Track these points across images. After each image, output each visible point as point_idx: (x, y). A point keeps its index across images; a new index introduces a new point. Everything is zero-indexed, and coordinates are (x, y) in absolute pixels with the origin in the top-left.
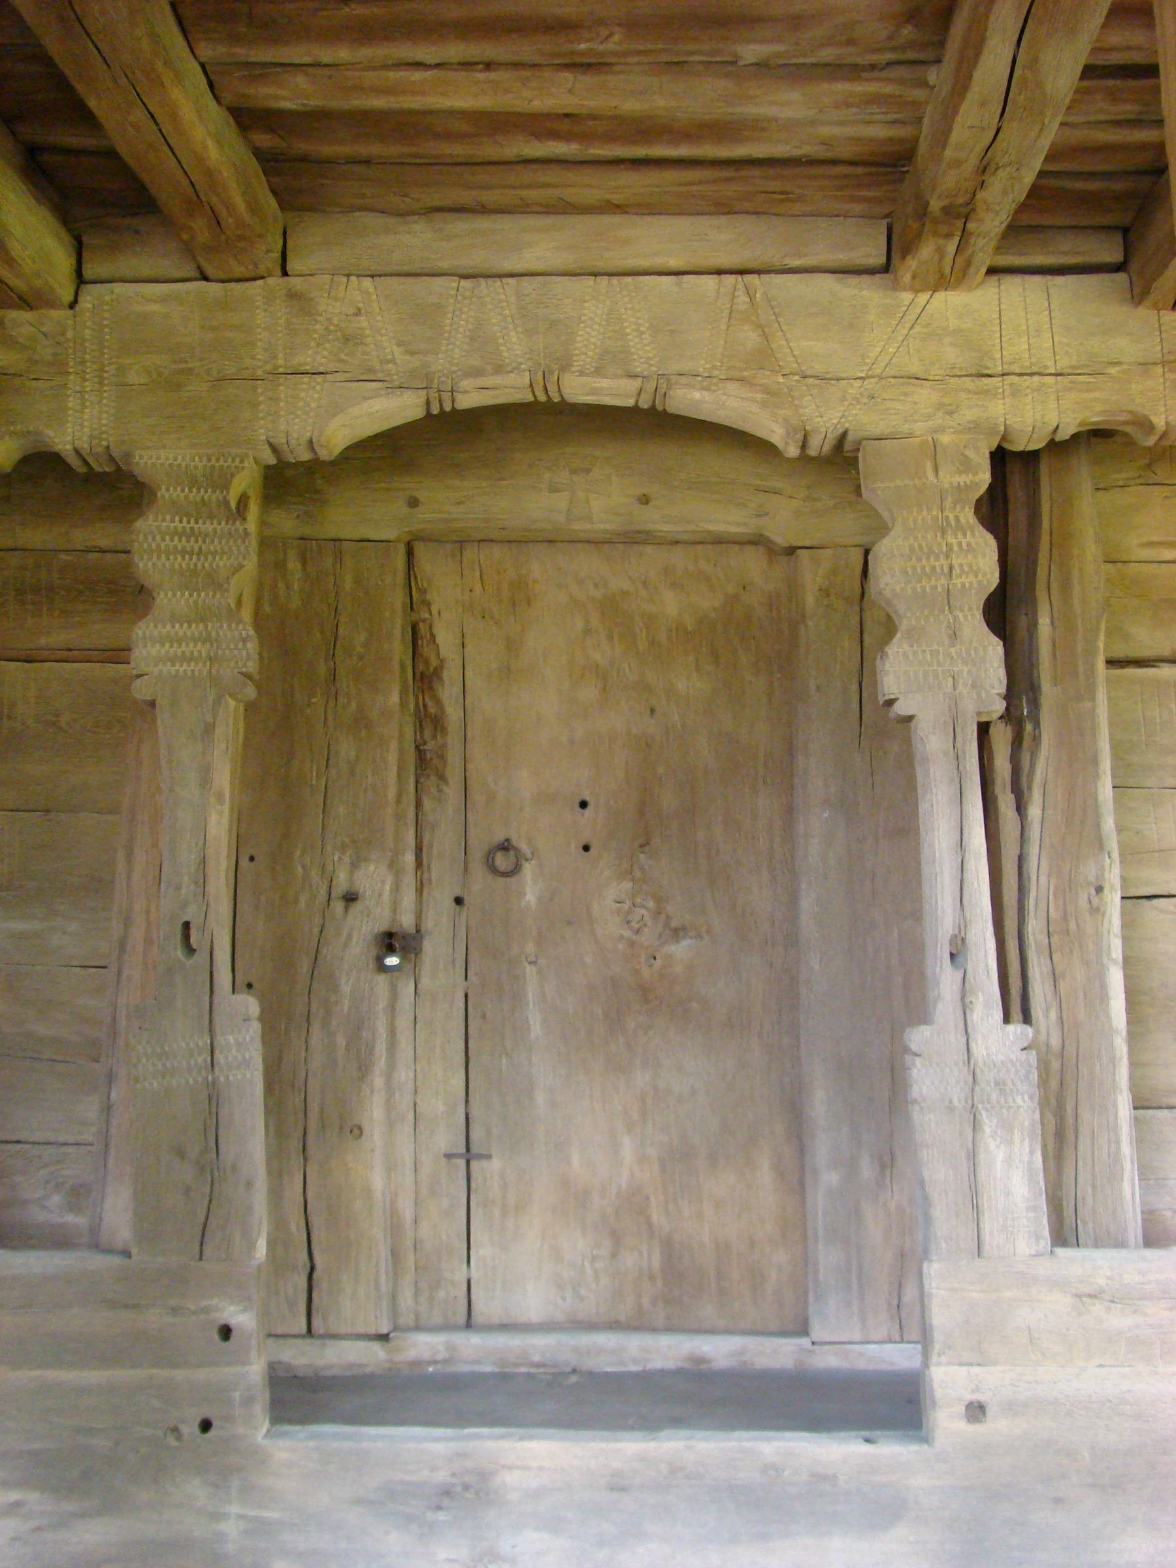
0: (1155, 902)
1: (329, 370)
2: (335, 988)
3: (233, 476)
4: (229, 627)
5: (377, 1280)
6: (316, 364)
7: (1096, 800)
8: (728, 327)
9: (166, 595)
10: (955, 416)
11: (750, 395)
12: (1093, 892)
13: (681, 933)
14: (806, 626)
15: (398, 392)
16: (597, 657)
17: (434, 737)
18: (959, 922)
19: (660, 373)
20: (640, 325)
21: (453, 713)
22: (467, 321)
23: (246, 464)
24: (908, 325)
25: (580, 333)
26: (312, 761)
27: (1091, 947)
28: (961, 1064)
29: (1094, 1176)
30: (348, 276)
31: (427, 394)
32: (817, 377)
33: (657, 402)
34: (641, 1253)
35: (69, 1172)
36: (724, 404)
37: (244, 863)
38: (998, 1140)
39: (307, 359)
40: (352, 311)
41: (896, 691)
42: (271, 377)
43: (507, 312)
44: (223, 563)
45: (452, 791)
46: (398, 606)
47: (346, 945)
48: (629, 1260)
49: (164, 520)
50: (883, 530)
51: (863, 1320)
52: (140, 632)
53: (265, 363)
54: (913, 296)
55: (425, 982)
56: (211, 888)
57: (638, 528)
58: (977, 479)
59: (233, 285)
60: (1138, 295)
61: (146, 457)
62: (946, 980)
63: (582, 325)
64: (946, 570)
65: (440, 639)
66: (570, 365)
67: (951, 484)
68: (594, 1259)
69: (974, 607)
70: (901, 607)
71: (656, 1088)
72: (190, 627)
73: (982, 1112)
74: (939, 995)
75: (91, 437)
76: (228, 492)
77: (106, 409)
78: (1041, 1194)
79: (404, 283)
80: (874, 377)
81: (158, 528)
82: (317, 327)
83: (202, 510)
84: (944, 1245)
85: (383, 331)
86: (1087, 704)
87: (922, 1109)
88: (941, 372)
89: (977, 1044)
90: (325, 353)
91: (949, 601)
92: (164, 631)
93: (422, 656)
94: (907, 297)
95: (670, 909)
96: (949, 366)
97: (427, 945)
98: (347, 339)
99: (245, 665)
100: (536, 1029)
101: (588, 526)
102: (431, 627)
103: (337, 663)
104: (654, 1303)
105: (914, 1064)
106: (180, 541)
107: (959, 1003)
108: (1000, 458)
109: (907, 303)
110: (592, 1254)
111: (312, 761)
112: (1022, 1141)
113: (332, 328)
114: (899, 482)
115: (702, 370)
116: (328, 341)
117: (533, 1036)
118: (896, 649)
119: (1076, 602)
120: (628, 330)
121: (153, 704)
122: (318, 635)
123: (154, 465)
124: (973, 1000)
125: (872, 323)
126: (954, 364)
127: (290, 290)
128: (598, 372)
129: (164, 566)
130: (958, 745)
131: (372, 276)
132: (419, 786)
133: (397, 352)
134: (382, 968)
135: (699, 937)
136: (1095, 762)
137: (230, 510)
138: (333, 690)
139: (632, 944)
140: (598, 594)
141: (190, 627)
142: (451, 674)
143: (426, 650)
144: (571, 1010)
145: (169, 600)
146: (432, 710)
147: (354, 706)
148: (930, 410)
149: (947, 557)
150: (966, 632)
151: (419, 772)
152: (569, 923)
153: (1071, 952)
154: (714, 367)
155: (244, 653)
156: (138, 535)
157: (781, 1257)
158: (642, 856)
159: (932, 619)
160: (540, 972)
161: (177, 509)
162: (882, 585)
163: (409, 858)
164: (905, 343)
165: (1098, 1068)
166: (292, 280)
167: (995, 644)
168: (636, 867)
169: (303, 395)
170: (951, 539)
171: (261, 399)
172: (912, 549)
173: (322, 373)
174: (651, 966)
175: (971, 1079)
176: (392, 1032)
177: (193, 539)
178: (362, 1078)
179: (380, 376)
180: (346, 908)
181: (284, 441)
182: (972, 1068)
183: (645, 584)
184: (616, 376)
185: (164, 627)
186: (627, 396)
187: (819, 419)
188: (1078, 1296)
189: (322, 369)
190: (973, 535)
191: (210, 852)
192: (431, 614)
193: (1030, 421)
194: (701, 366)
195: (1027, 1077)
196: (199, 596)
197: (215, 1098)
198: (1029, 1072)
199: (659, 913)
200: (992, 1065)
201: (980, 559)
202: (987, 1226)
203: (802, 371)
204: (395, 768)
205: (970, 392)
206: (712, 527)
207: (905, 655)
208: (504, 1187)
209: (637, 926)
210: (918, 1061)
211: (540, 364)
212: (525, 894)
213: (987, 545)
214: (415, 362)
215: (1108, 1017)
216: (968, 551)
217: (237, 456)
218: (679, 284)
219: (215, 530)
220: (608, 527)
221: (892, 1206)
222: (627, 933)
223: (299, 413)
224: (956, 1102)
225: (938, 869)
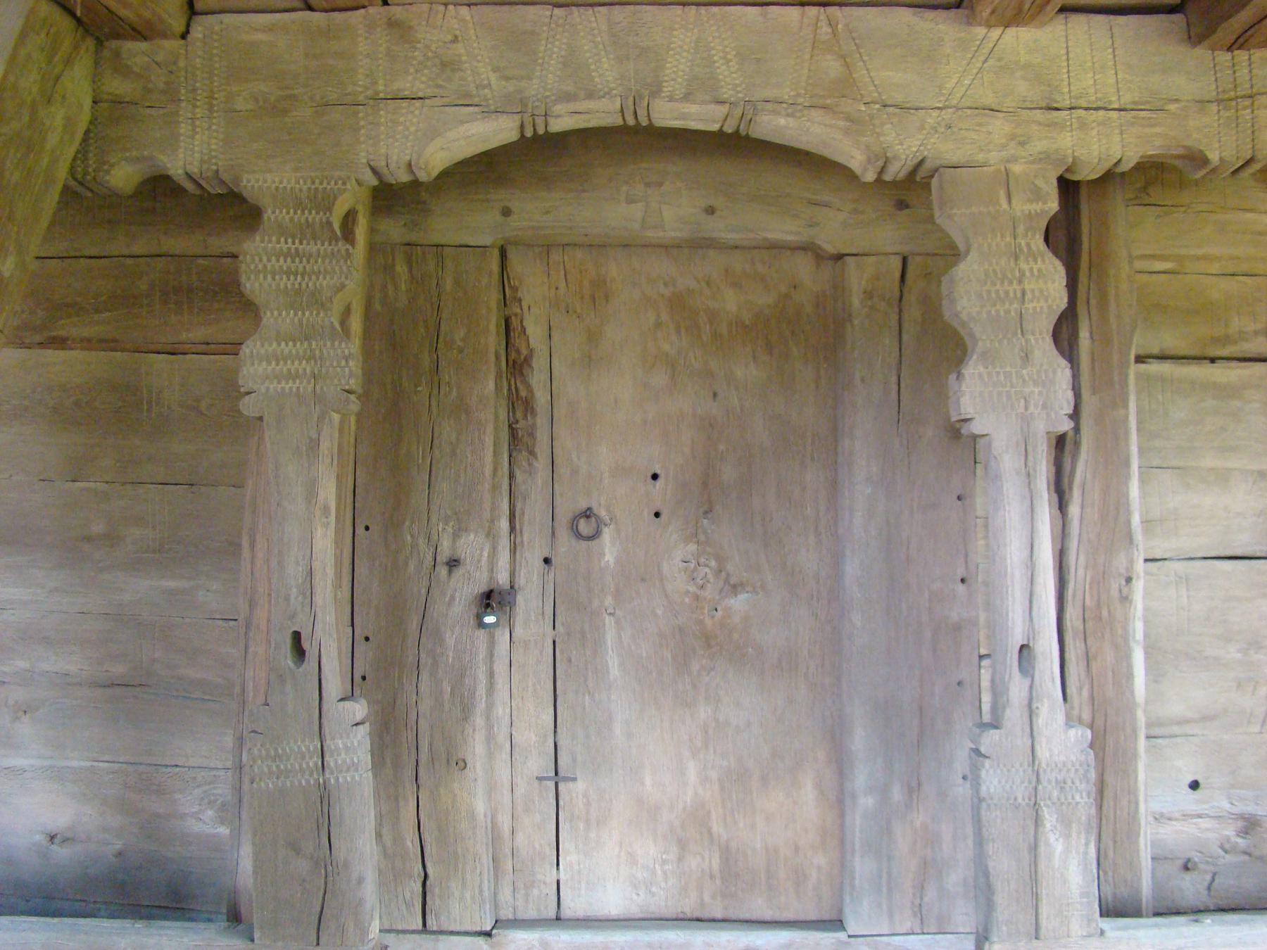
1: (427, 95)
2: (440, 640)
3: (335, 198)
4: (333, 345)
5: (480, 886)
6: (414, 90)
7: (1128, 499)
8: (812, 56)
9: (272, 314)
10: (1027, 146)
11: (834, 122)
12: (1123, 582)
13: (739, 589)
14: (852, 326)
15: (493, 116)
16: (666, 347)
17: (525, 417)
18: (1029, 631)
19: (747, 99)
20: (727, 53)
21: (541, 398)
22: (560, 48)
23: (348, 186)
24: (982, 59)
25: (670, 60)
26: (418, 443)
27: (1120, 632)
28: (1026, 764)
29: (1115, 832)
30: (446, 5)
31: (522, 117)
33: (741, 127)
34: (703, 859)
35: (219, 791)
36: (808, 130)
37: (360, 530)
38: (1058, 833)
39: (406, 84)
40: (450, 38)
41: (972, 411)
42: (371, 102)
43: (599, 39)
44: (324, 282)
45: (542, 464)
46: (493, 305)
47: (450, 604)
48: (693, 863)
49: (270, 241)
51: (891, 915)
52: (247, 351)
53: (367, 88)
54: (986, 31)
55: (519, 631)
56: (318, 600)
57: (707, 235)
58: (1046, 207)
59: (336, 14)
60: (1196, 38)
61: (253, 182)
62: (1017, 688)
63: (671, 52)
64: (1019, 294)
65: (529, 331)
66: (660, 90)
67: (1023, 211)
68: (664, 862)
69: (1045, 330)
70: (977, 330)
71: (717, 720)
72: (295, 345)
73: (1044, 808)
74: (1008, 700)
75: (202, 162)
76: (331, 213)
77: (215, 134)
78: (1094, 881)
79: (499, 12)
80: (951, 108)
81: (265, 249)
82: (416, 54)
83: (306, 232)
84: (1004, 928)
85: (479, 58)
86: (1122, 412)
87: (989, 806)
88: (1014, 104)
89: (1041, 747)
90: (424, 79)
91: (1021, 325)
92: (270, 349)
93: (514, 346)
94: (980, 31)
95: (730, 567)
96: (1021, 99)
97: (520, 599)
98: (444, 65)
99: (348, 384)
100: (615, 671)
101: (661, 234)
102: (521, 322)
103: (440, 356)
104: (713, 897)
105: (983, 766)
106: (285, 262)
107: (1026, 709)
108: (1068, 187)
109: (980, 37)
110: (662, 858)
111: (418, 443)
112: (1079, 833)
113: (430, 54)
114: (974, 209)
115: (787, 97)
116: (426, 67)
117: (611, 677)
118: (972, 369)
119: (1112, 319)
120: (715, 58)
121: (261, 419)
122: (422, 330)
123: (260, 188)
124: (1040, 706)
125: (948, 55)
126: (1026, 97)
127: (390, 19)
128: (687, 97)
129: (270, 286)
130: (1030, 464)
131: (469, 5)
132: (512, 460)
133: (493, 78)
134: (481, 625)
135: (754, 591)
136: (1127, 464)
137: (333, 231)
138: (436, 378)
139: (697, 598)
140: (667, 292)
141: (295, 345)
142: (539, 363)
143: (518, 342)
144: (644, 655)
145: (276, 319)
146: (523, 394)
147: (454, 394)
148: (1004, 141)
149: (1020, 282)
150: (1037, 355)
151: (511, 447)
152: (643, 580)
153: (1103, 635)
154: (798, 95)
155: (347, 370)
156: (245, 256)
157: (821, 860)
158: (705, 521)
159: (1005, 342)
160: (618, 622)
161: (282, 231)
162: (959, 308)
163: (504, 524)
164: (979, 75)
165: (1123, 738)
166: (392, 9)
167: (1064, 366)
168: (700, 530)
169: (402, 119)
170: (1024, 266)
171: (362, 123)
172: (986, 273)
173: (421, 98)
174: (713, 617)
175: (1034, 779)
176: (491, 675)
177: (297, 260)
178: (465, 719)
179: (476, 101)
180: (450, 572)
181: (383, 163)
182: (1036, 768)
183: (708, 283)
184: (704, 102)
185: (270, 345)
186: (714, 121)
187: (900, 147)
189: (420, 94)
190: (1043, 261)
191: (316, 565)
192: (522, 309)
193: (1096, 154)
194: (786, 93)
195: (1085, 776)
196: (304, 314)
197: (326, 798)
198: (1087, 771)
199: (721, 571)
200: (1053, 766)
201: (1049, 285)
202: (1044, 910)
203: (882, 100)
204: (491, 449)
205: (1040, 124)
206: (770, 236)
207: (980, 375)
208: (588, 804)
209: (701, 582)
210: (987, 763)
211: (630, 90)
212: (604, 555)
213: (1056, 272)
214: (511, 87)
215: (1132, 692)
216: (1039, 277)
217: (340, 178)
219: (319, 250)
220: (678, 234)
221: (918, 824)
222: (692, 589)
223: (398, 137)
224: (1020, 800)
225: (1009, 583)
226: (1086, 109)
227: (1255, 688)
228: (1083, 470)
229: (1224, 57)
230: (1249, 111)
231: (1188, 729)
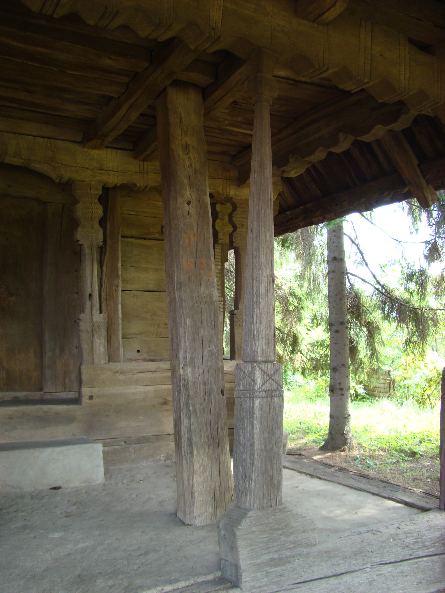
0: (125, 292)
32: (65, 165)
50: (77, 202)
60: (136, 157)
62: (88, 304)
84: (85, 362)
94: (86, 150)
118: (80, 229)
149: (92, 209)
170: (93, 206)
188: (114, 372)
195: (104, 325)
202: (95, 357)
210: (81, 321)
218: (370, 281)
226: (110, 171)
227: (154, 326)
228: (107, 258)
229: (142, 163)
230: (146, 176)
231: (137, 336)
